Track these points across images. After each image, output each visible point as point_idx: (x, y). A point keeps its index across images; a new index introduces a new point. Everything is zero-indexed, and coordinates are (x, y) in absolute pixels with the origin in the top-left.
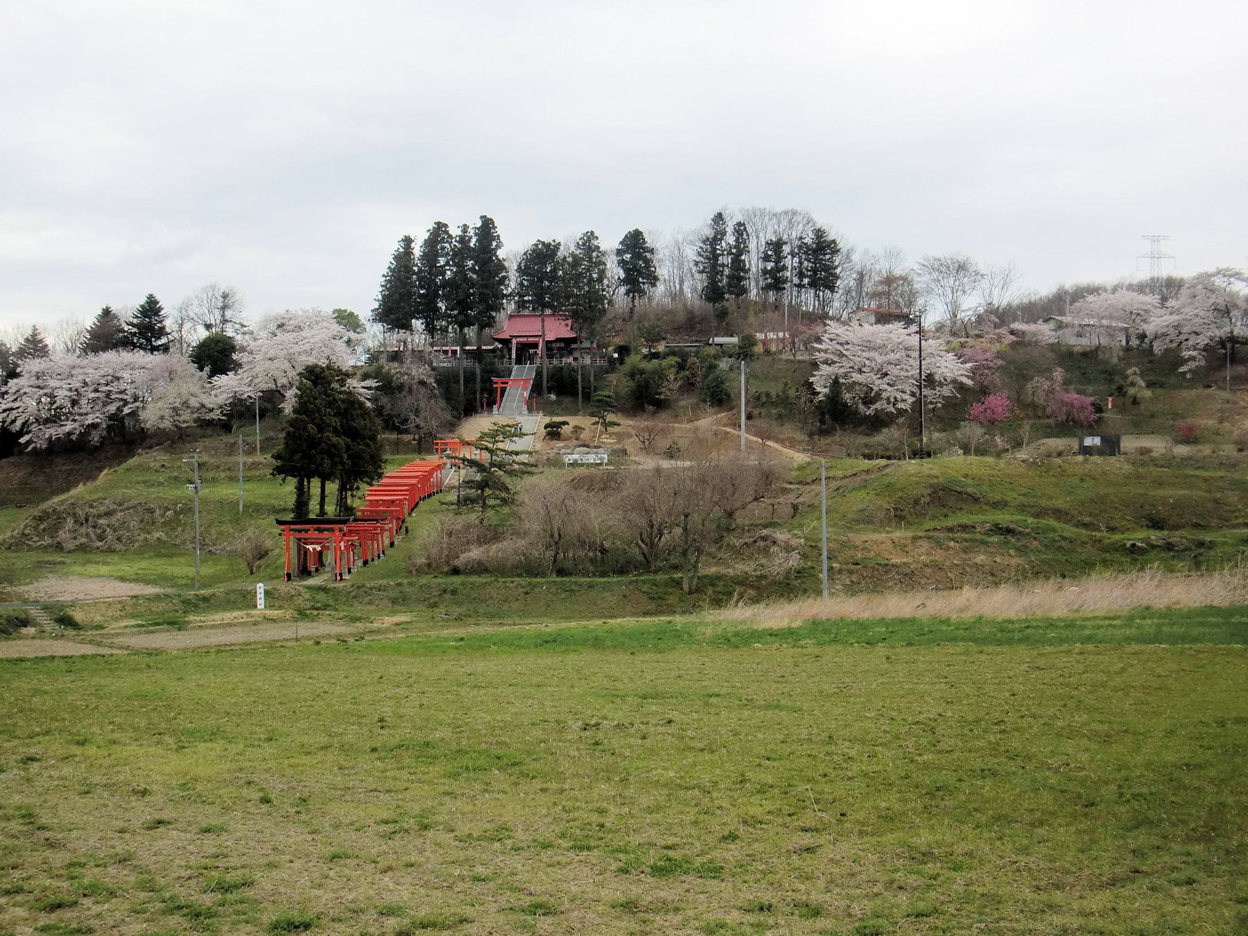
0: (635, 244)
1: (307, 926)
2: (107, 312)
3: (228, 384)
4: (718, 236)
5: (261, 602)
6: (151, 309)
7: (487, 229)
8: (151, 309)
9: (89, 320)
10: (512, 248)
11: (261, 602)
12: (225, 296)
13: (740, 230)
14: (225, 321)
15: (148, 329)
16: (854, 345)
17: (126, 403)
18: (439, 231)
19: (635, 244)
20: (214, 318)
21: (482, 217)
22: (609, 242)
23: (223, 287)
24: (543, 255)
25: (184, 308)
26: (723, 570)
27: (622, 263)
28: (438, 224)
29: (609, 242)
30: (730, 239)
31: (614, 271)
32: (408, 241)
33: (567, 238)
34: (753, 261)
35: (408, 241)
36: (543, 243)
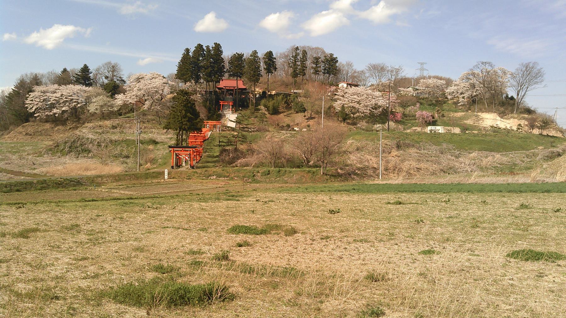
0: (269, 55)
1: (207, 296)
2: (65, 70)
3: (120, 99)
4: (297, 55)
5: (166, 177)
6: (85, 69)
7: (218, 47)
8: (85, 69)
9: (59, 71)
10: (227, 54)
11: (166, 177)
12: (113, 67)
13: (305, 53)
14: (113, 76)
15: (84, 77)
16: (346, 96)
17: (79, 103)
18: (200, 47)
19: (269, 55)
20: (110, 74)
21: (215, 44)
22: (261, 54)
23: (113, 63)
24: (238, 59)
25: (98, 70)
26: (387, 182)
27: (265, 62)
28: (199, 45)
29: (261, 54)
30: (301, 55)
31: (262, 66)
32: (187, 50)
33: (247, 53)
34: (309, 63)
35: (187, 50)
36: (238, 54)
